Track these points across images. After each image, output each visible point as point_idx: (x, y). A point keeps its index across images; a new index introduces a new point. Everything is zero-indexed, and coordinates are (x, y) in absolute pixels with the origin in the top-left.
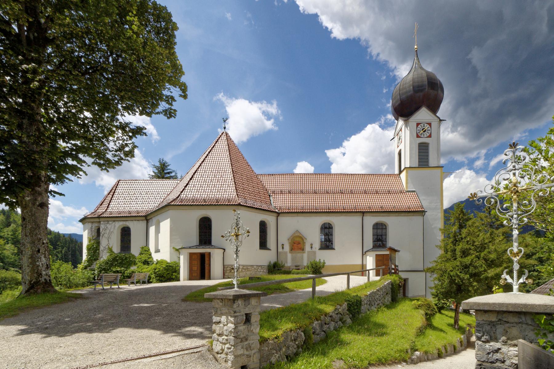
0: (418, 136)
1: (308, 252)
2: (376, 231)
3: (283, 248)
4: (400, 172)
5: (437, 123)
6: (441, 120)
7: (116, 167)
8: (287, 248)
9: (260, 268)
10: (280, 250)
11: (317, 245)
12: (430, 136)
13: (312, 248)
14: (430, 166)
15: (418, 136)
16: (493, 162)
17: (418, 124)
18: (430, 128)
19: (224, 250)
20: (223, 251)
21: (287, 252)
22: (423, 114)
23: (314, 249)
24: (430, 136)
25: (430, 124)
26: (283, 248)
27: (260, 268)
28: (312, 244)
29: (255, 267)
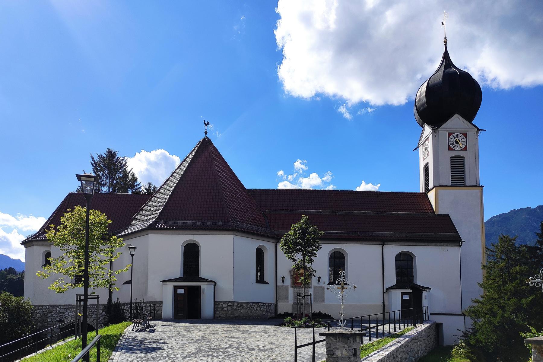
0: (450, 149)
1: (315, 287)
2: (399, 263)
3: (283, 281)
4: (427, 190)
5: (474, 132)
6: (479, 130)
7: (474, 304)
8: (288, 282)
9: (256, 305)
10: (280, 283)
11: (325, 279)
12: (465, 149)
13: (319, 281)
14: (467, 184)
15: (450, 149)
16: (356, 330)
17: (450, 134)
18: (465, 139)
19: (215, 283)
20: (213, 284)
21: (288, 286)
22: (456, 122)
23: (321, 284)
24: (465, 149)
25: (465, 135)
26: (283, 281)
27: (256, 305)
28: (319, 278)
29: (251, 304)
